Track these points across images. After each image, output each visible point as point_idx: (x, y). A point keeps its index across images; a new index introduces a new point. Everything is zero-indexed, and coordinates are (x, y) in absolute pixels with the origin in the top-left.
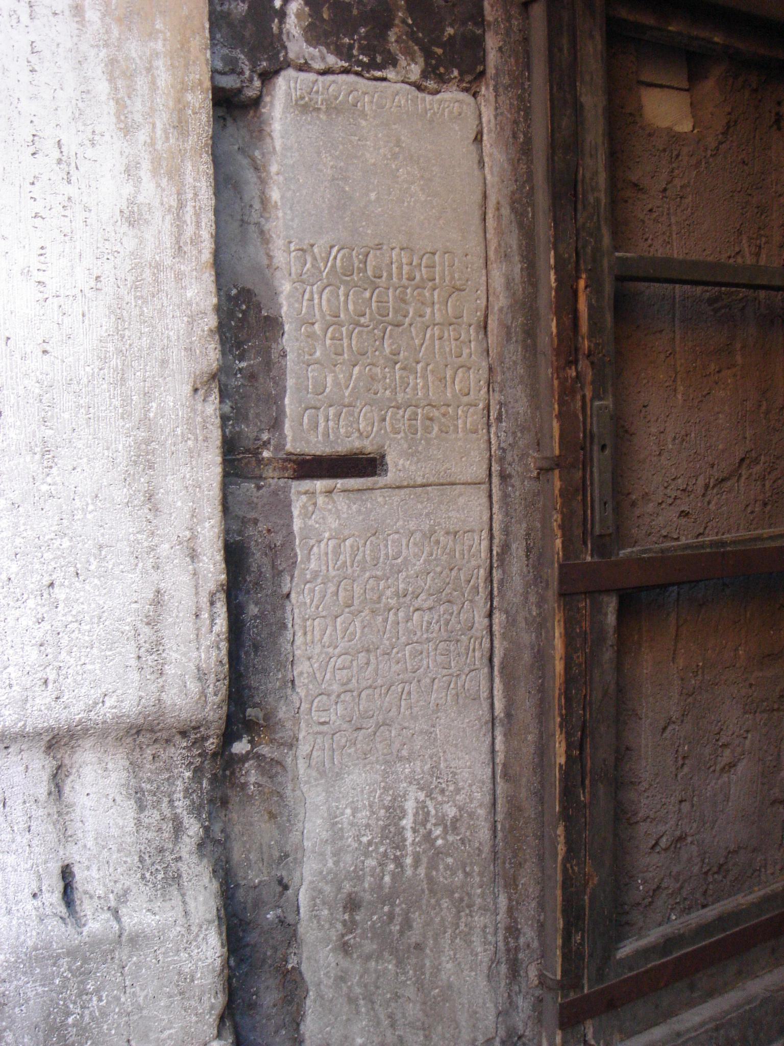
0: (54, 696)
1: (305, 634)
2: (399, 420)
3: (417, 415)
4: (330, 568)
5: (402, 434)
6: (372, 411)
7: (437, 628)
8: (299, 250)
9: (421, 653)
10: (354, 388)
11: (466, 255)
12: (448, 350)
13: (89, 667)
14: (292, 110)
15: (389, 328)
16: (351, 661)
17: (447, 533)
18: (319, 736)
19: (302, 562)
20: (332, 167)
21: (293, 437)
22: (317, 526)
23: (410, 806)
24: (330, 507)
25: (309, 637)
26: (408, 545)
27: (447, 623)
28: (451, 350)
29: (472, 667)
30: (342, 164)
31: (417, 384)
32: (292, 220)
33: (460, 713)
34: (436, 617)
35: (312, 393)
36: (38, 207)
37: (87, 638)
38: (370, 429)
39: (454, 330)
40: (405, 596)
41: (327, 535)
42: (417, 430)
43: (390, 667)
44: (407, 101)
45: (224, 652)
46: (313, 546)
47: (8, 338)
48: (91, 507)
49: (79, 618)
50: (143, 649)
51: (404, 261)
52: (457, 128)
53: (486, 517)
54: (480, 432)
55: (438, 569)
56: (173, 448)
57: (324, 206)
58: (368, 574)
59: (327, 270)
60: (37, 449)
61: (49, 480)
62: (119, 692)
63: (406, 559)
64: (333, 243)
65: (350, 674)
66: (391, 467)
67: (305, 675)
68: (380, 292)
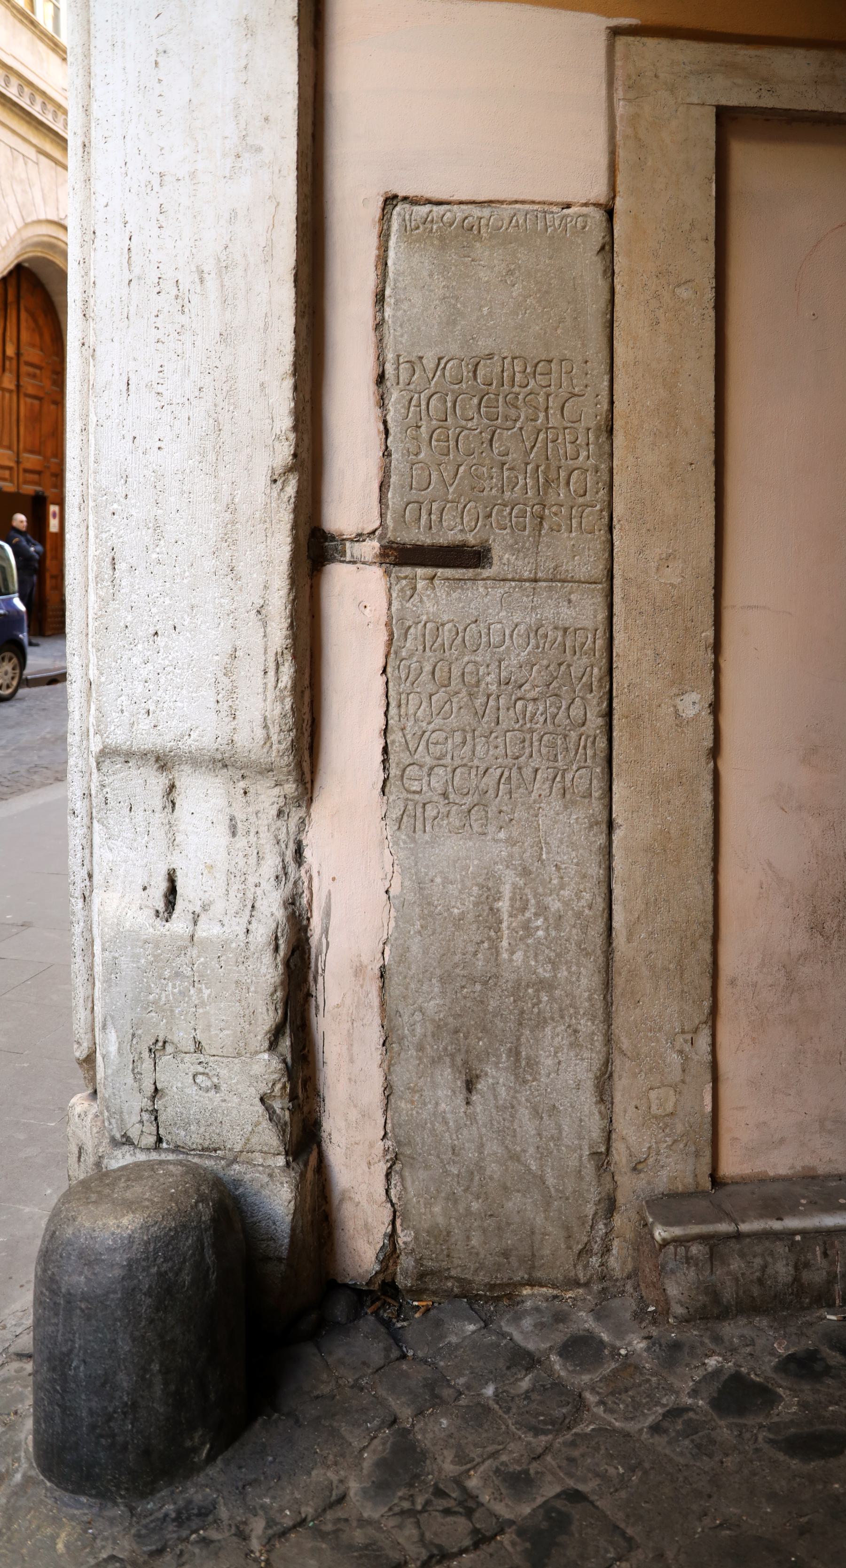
0: (152, 725)
1: (399, 706)
2: (505, 517)
3: (526, 512)
4: (427, 649)
5: (508, 530)
6: (476, 507)
7: (542, 719)
8: (407, 362)
10: (458, 485)
12: (561, 452)
13: (179, 704)
17: (556, 628)
23: (507, 890)
24: (429, 592)
25: (403, 711)
26: (511, 636)
29: (582, 764)
30: (454, 284)
31: (526, 484)
32: (402, 336)
33: (566, 807)
35: (415, 489)
36: (160, 334)
37: (179, 680)
38: (473, 523)
39: (570, 433)
40: (507, 683)
42: (525, 527)
43: (488, 750)
45: (288, 707)
46: (409, 627)
47: (135, 438)
48: (187, 574)
49: (174, 664)
50: (221, 695)
51: (517, 369)
52: (580, 241)
54: (597, 533)
55: (545, 662)
56: (252, 529)
57: (434, 322)
58: (466, 659)
59: (435, 379)
60: (151, 525)
61: (158, 550)
62: (201, 728)
63: (508, 648)
65: (444, 750)
67: (397, 744)
68: (489, 398)
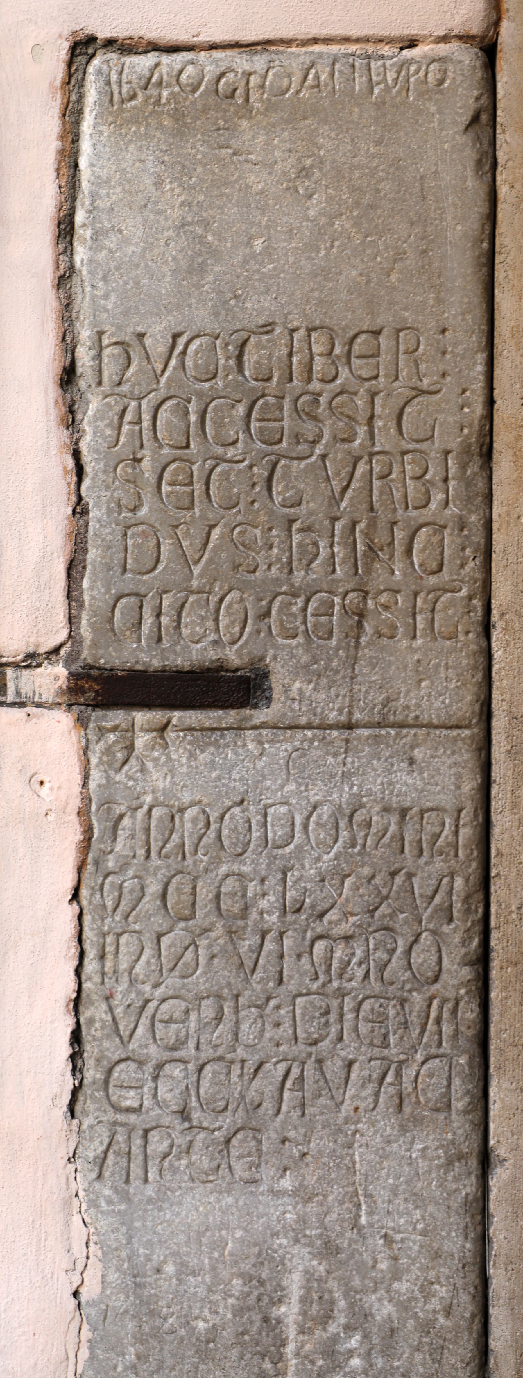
1: (102, 957)
6: (242, 600)
7: (360, 973)
8: (116, 343)
9: (327, 1012)
10: (210, 561)
11: (444, 331)
14: (111, 119)
15: (283, 462)
16: (187, 1012)
18: (119, 1129)
19: (101, 839)
20: (183, 204)
21: (92, 640)
22: (131, 783)
24: (156, 754)
25: (109, 964)
26: (305, 827)
27: (383, 967)
28: (406, 496)
29: (433, 1051)
30: (201, 198)
31: (333, 555)
32: (106, 296)
33: (403, 1130)
34: (359, 953)
38: (237, 629)
39: (413, 461)
40: (298, 910)
41: (148, 799)
44: (332, 75)
46: (121, 816)
53: (470, 784)
54: (461, 637)
55: (366, 871)
57: (165, 269)
58: (223, 869)
59: (167, 374)
63: (299, 848)
64: (179, 329)
65: (183, 1033)
66: (277, 692)
67: (98, 1025)
68: (266, 404)
